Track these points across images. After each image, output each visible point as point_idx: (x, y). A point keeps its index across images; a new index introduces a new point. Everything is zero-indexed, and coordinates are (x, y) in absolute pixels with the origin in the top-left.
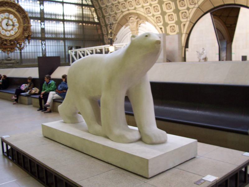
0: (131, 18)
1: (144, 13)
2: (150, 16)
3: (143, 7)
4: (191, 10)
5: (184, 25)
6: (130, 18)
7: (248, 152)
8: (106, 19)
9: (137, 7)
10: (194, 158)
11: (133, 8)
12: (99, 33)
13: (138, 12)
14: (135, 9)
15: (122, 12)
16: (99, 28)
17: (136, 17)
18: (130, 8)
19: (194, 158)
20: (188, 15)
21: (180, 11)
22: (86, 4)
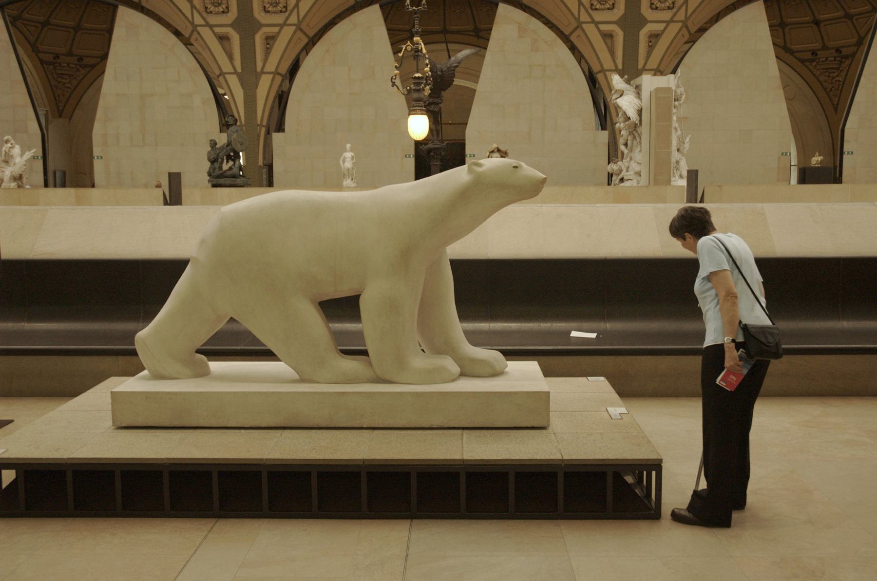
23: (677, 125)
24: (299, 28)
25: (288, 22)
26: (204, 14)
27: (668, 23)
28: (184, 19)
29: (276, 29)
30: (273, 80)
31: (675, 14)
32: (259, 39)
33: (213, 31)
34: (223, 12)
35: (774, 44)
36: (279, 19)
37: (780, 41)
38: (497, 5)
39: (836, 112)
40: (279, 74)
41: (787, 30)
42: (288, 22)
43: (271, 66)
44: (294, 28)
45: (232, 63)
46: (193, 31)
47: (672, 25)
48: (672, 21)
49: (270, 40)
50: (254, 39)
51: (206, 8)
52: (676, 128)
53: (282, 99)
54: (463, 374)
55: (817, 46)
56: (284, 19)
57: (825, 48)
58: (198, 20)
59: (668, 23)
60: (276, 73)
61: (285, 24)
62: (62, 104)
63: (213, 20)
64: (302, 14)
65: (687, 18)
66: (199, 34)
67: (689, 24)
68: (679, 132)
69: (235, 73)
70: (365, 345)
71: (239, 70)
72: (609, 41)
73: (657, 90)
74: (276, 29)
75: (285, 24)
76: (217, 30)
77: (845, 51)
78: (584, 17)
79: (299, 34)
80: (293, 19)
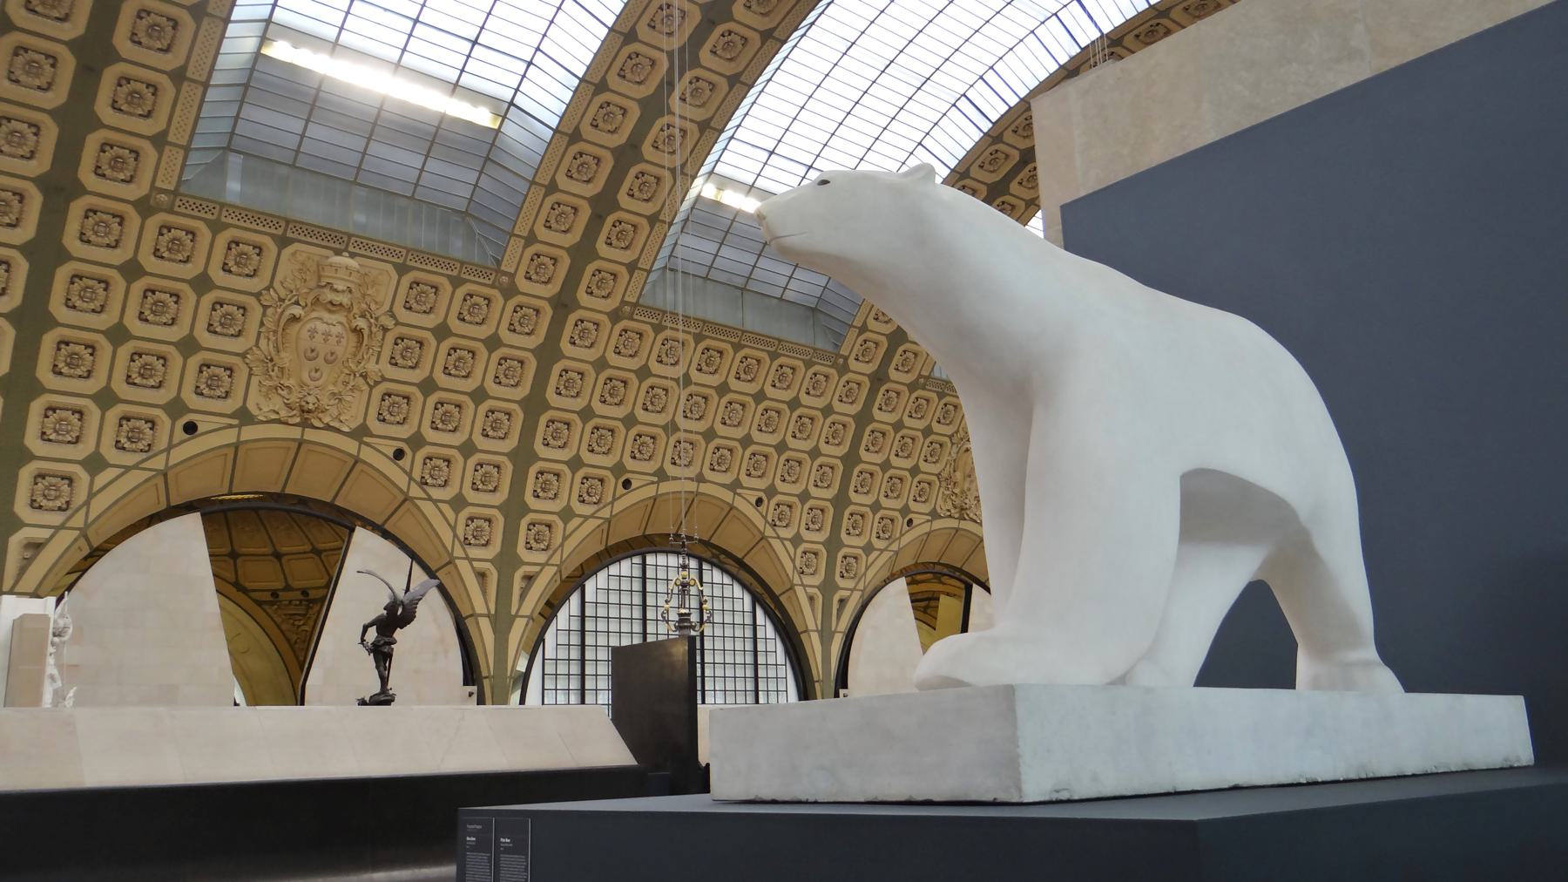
11: (727, 479)
20: (558, 540)
23: (55, 672)
24: (84, 533)
27: (57, 529)
29: (537, 569)
35: (215, 575)
36: (541, 558)
37: (230, 576)
38: (352, 530)
41: (239, 561)
44: (77, 533)
47: (63, 532)
48: (62, 527)
49: (529, 579)
52: (52, 677)
55: (279, 585)
57: (288, 588)
59: (57, 529)
60: (531, 618)
61: (547, 564)
63: (474, 552)
64: (92, 517)
67: (91, 533)
68: (59, 683)
69: (488, 616)
73: (23, 617)
74: (537, 569)
75: (547, 564)
76: (476, 564)
77: (312, 594)
78: (458, 552)
79: (82, 542)
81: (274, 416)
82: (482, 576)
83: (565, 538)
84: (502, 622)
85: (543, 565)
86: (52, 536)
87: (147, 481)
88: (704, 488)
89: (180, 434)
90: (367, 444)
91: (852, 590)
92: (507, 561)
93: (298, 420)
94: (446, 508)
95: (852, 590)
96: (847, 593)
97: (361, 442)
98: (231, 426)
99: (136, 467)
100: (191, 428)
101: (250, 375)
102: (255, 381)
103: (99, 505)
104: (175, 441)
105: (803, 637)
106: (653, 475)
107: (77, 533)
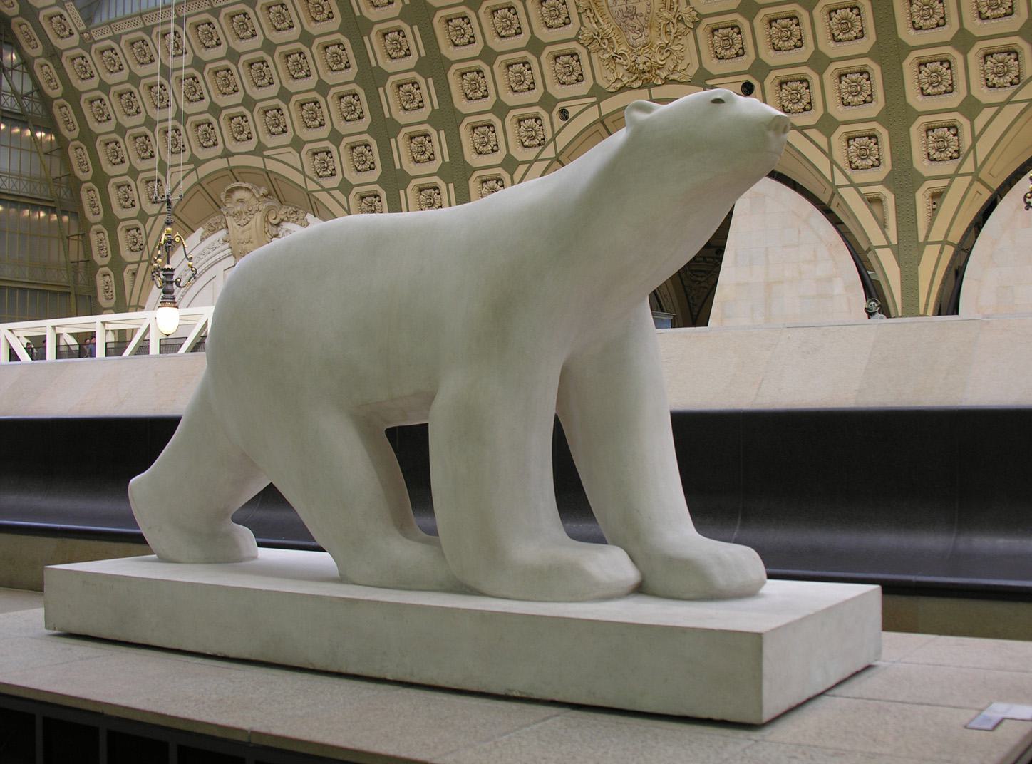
0: (239, 195)
1: (303, 173)
2: (328, 191)
3: (297, 144)
4: (151, 220)
5: (937, 196)
6: (231, 191)
7: (1029, 639)
8: (112, 191)
9: (270, 141)
10: (868, 667)
11: (251, 145)
12: (74, 258)
13: (272, 166)
14: (260, 150)
15: (196, 162)
16: (75, 231)
17: (263, 191)
18: (233, 146)
19: (868, 667)
20: (967, 141)
21: (371, 24)
22: (16, 109)
24: (976, 177)
25: (961, 171)
26: (848, 171)
28: (821, 179)
29: (945, 182)
30: (941, 253)
31: (960, 165)
32: (922, 199)
33: (859, 192)
34: (873, 166)
36: (949, 168)
39: (9, 330)
40: (949, 243)
42: (961, 171)
43: (937, 235)
44: (970, 178)
45: (885, 234)
46: (833, 194)
50: (914, 197)
51: (851, 163)
53: (957, 273)
54: (640, 589)
56: (955, 167)
58: (840, 179)
60: (945, 242)
62: (697, 309)
63: (858, 177)
64: (980, 159)
65: (978, 169)
66: (841, 197)
69: (889, 245)
70: (139, 529)
71: (894, 242)
72: (876, 208)
74: (945, 182)
76: (864, 190)
80: (968, 167)
81: (619, 85)
82: (874, 201)
83: (975, 139)
84: (908, 251)
85: (951, 177)
86: (950, 184)
87: (1022, 113)
88: (235, 161)
89: (558, 123)
90: (268, 157)
91: (138, 263)
92: (904, 180)
93: (639, 83)
94: (337, 194)
95: (138, 263)
96: (135, 266)
97: (264, 157)
98: (592, 104)
99: (1008, 101)
100: (564, 114)
101: (589, 53)
102: (594, 56)
103: (983, 148)
104: (556, 130)
105: (870, 256)
106: (188, 163)
107: (970, 178)
